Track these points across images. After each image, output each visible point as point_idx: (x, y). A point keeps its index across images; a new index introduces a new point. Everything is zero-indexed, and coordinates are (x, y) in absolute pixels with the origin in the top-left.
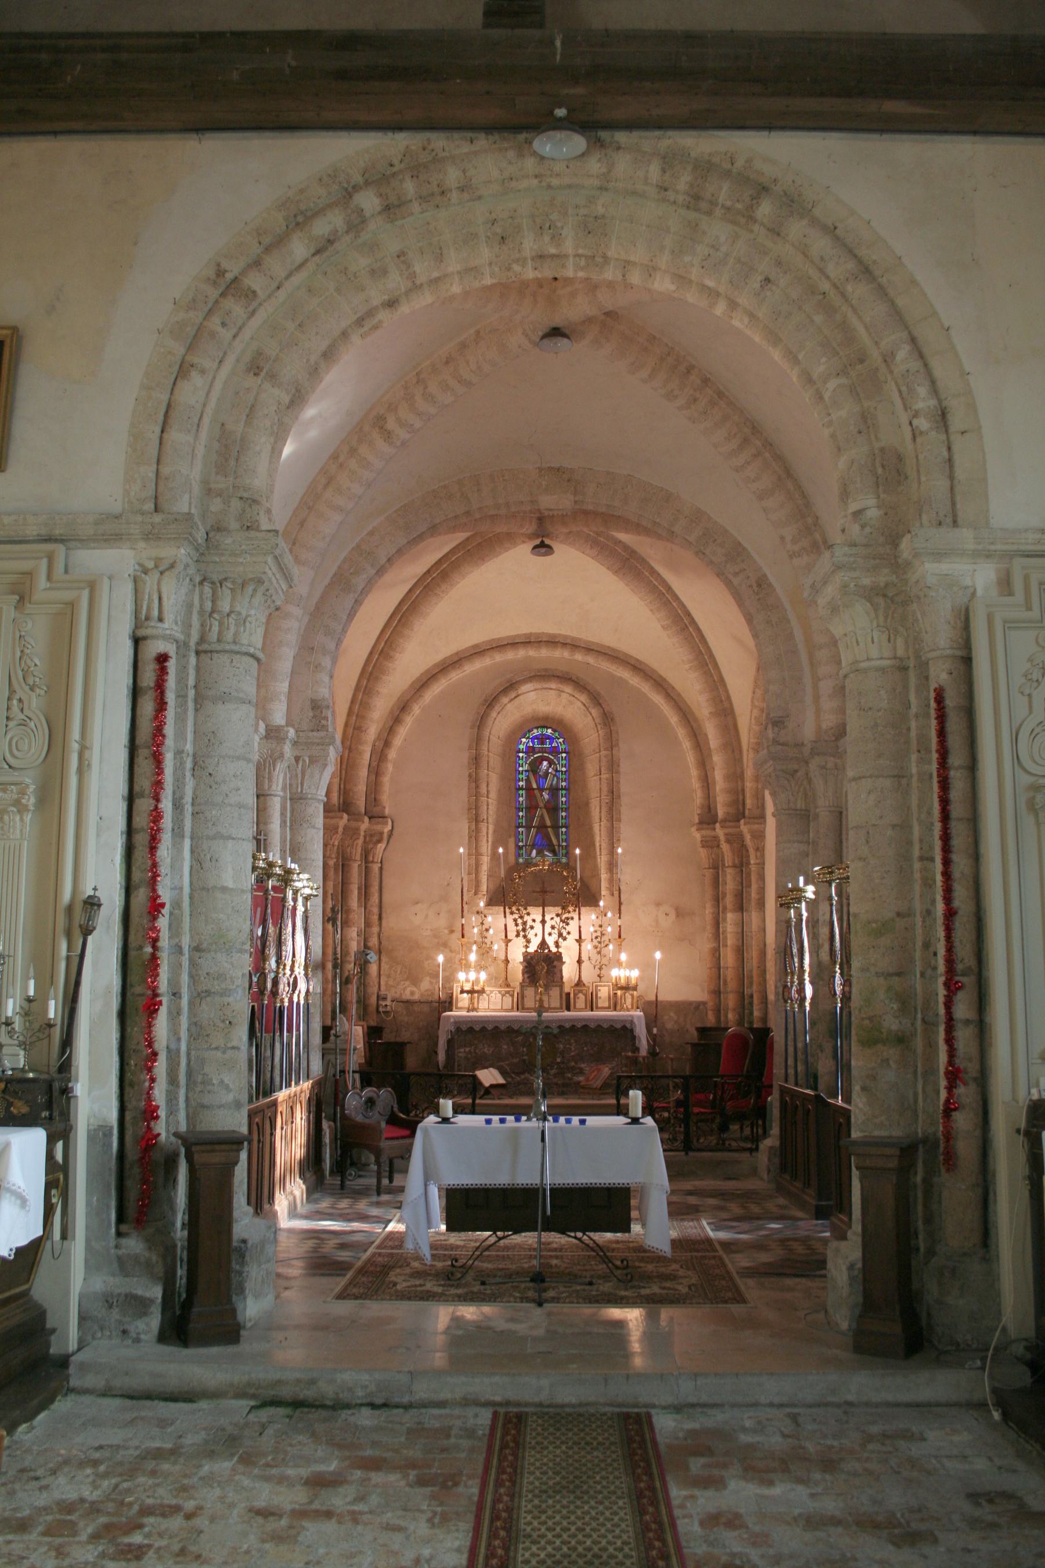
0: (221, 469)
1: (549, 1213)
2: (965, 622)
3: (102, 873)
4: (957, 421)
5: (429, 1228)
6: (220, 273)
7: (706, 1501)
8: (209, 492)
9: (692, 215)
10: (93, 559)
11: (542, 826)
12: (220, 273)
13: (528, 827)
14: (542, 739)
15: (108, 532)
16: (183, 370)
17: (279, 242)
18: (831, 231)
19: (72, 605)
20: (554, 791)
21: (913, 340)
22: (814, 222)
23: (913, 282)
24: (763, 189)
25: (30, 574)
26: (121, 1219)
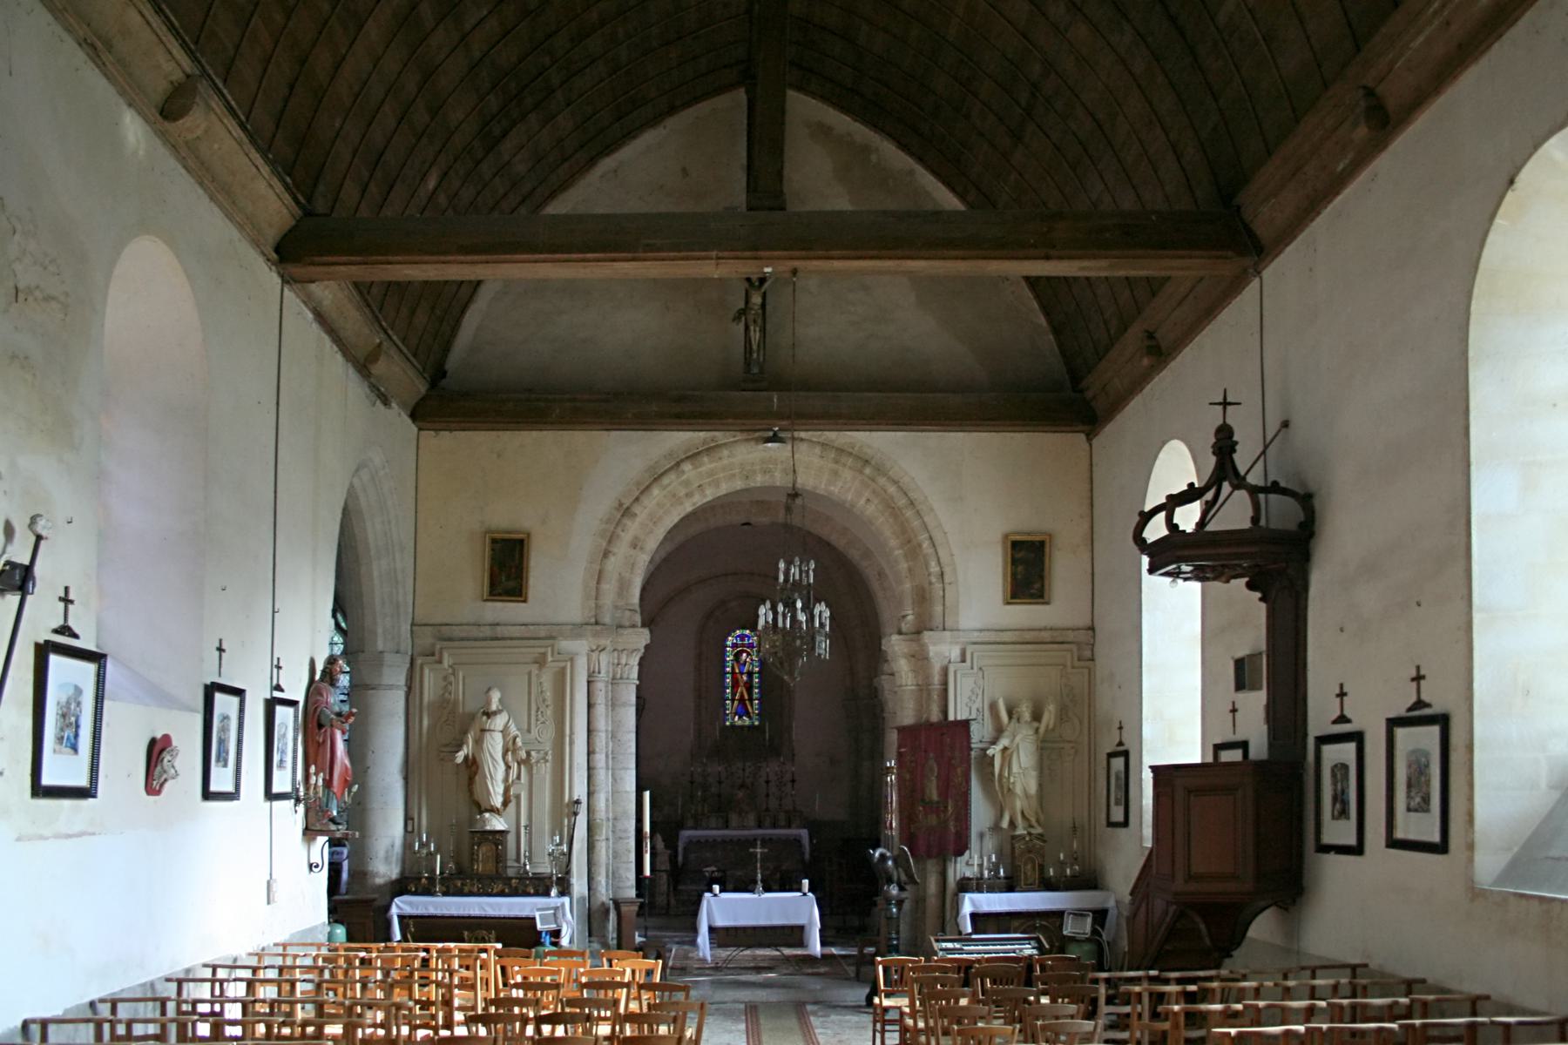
1: (647, 872)
2: (945, 672)
3: (580, 791)
5: (1164, 1034)
6: (621, 505)
8: (616, 607)
9: (835, 466)
10: (566, 645)
11: (742, 700)
12: (621, 505)
13: (733, 700)
14: (742, 637)
15: (577, 630)
16: (606, 554)
18: (895, 482)
19: (564, 669)
23: (932, 510)
24: (867, 462)
25: (544, 654)
26: (590, 935)
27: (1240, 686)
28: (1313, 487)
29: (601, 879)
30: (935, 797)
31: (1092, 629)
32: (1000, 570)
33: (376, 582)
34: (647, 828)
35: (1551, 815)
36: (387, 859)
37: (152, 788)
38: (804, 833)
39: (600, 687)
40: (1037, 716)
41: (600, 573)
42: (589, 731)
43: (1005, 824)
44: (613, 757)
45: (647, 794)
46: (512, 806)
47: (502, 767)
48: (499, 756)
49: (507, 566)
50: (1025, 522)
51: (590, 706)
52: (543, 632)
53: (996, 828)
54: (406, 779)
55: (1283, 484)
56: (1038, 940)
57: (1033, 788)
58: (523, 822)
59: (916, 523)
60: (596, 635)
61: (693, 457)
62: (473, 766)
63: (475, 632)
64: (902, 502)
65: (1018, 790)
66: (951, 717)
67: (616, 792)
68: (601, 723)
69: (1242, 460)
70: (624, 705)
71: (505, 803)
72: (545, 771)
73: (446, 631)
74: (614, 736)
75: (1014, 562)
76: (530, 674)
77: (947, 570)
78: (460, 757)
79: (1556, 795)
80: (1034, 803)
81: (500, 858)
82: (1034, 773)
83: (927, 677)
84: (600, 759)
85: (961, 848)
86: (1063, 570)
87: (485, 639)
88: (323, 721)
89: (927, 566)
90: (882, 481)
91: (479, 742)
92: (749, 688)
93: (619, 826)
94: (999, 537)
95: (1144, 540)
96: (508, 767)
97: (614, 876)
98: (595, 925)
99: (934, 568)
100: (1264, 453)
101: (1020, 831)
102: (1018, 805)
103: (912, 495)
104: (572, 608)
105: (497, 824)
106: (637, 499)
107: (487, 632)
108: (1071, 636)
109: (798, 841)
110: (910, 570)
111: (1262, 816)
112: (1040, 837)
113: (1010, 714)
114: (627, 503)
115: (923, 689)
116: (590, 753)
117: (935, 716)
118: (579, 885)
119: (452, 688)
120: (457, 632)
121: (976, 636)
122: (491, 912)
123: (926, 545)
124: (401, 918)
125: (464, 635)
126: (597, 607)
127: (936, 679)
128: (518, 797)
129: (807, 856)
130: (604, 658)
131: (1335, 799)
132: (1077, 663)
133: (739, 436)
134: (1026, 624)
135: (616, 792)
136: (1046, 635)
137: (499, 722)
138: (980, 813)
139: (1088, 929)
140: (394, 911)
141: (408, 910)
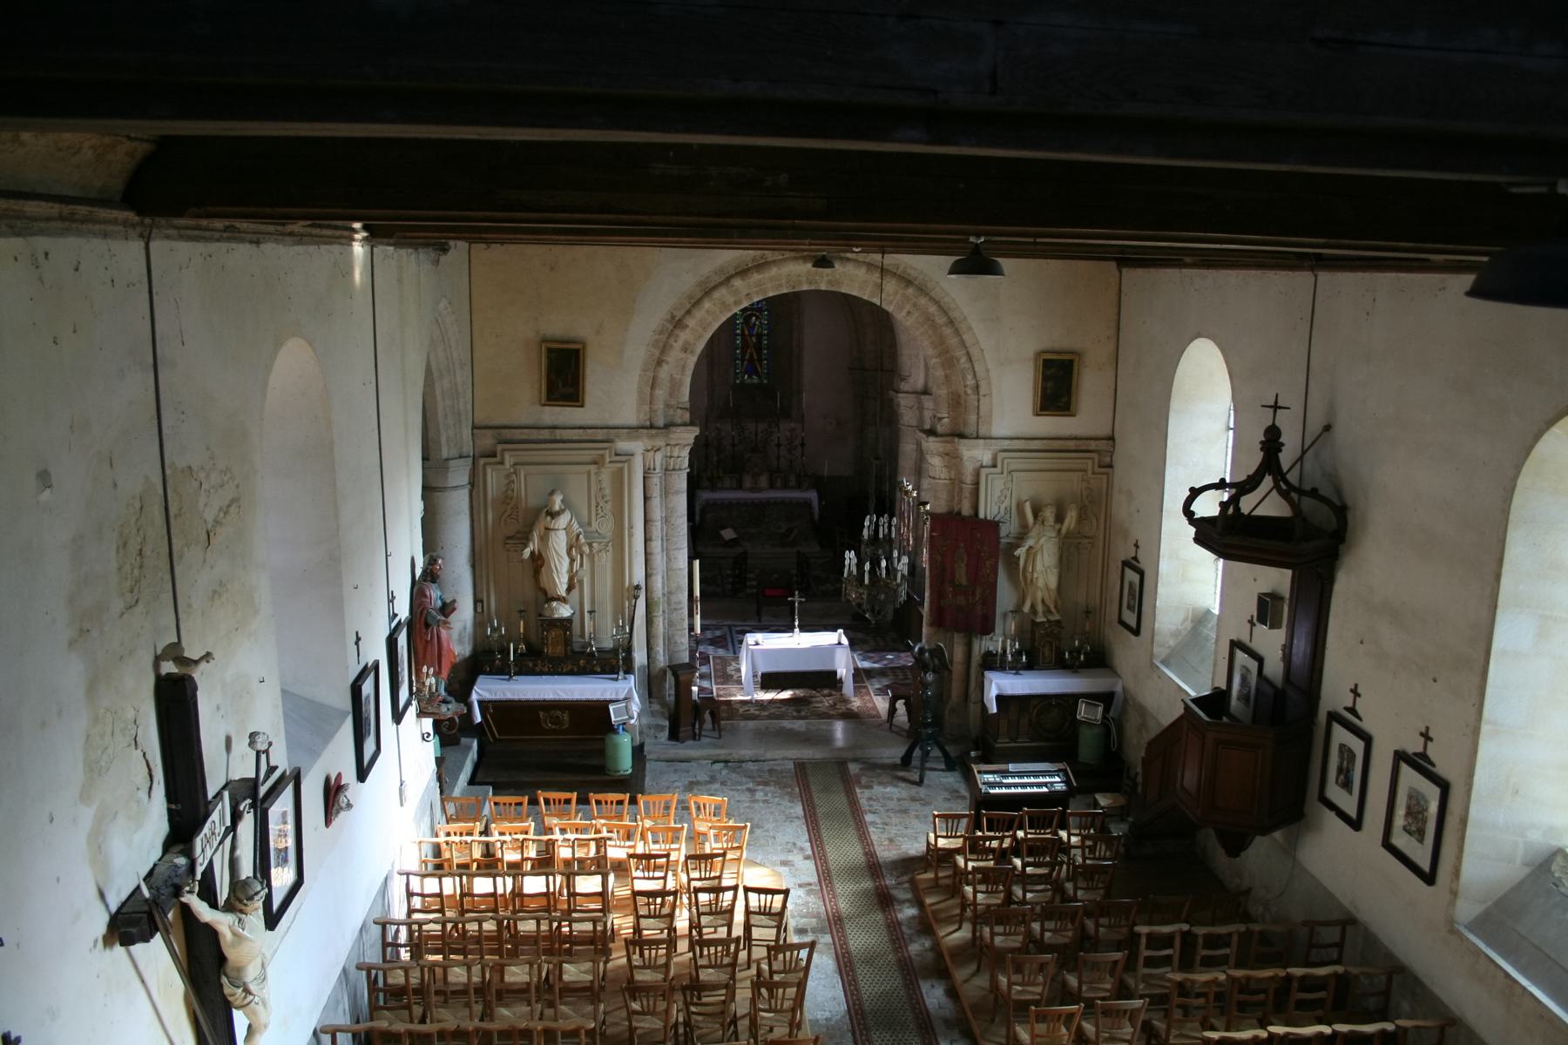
0: (671, 395)
2: (977, 474)
3: (639, 576)
4: (982, 391)
6: (673, 317)
7: (867, 793)
10: (623, 445)
11: (751, 360)
13: (743, 360)
15: (634, 430)
16: (659, 363)
17: (698, 302)
18: (937, 303)
19: (621, 469)
20: (759, 336)
21: (968, 354)
22: (931, 299)
23: (970, 328)
25: (602, 456)
26: (650, 696)
27: (1262, 618)
28: (1349, 504)
29: (660, 649)
30: (964, 581)
31: (1112, 438)
32: (1031, 385)
33: (439, 397)
34: (697, 593)
35: (1521, 884)
36: (460, 641)
37: (328, 822)
38: (812, 495)
39: (655, 480)
40: (1060, 518)
41: (654, 379)
42: (646, 522)
43: (1026, 609)
44: (667, 539)
45: (697, 563)
46: (575, 592)
47: (567, 560)
48: (563, 552)
49: (564, 373)
50: (1057, 339)
51: (646, 499)
52: (600, 434)
53: (1017, 610)
54: (473, 566)
55: (1321, 492)
56: (1064, 771)
57: (1053, 582)
58: (587, 608)
59: (954, 341)
60: (652, 437)
61: (743, 272)
62: (538, 561)
63: (534, 434)
64: (941, 320)
65: (1041, 583)
66: (982, 516)
67: (669, 570)
68: (657, 513)
69: (1286, 458)
70: (677, 492)
71: (569, 590)
72: (606, 560)
73: (507, 434)
74: (667, 520)
75: (1045, 378)
76: (589, 473)
77: (983, 385)
78: (527, 553)
79: (1527, 870)
80: (1054, 594)
81: (568, 642)
82: (1055, 571)
83: (960, 473)
84: (656, 545)
85: (987, 628)
86: (1090, 385)
87: (546, 442)
88: (430, 620)
89: (964, 378)
90: (923, 301)
91: (544, 539)
92: (759, 349)
93: (674, 599)
94: (1031, 355)
95: (1193, 513)
96: (572, 561)
97: (669, 641)
98: (654, 690)
99: (970, 381)
100: (1301, 458)
101: (1040, 619)
102: (1039, 595)
103: (954, 314)
104: (628, 411)
105: (564, 611)
106: (689, 312)
107: (546, 434)
108: (1093, 445)
109: (807, 504)
110: (946, 377)
111: (1275, 739)
112: (1058, 622)
113: (1036, 516)
114: (679, 315)
115: (956, 482)
116: (647, 540)
117: (966, 510)
118: (640, 657)
119: (515, 486)
120: (517, 434)
121: (1006, 444)
122: (564, 696)
123: (963, 360)
124: (481, 703)
125: (524, 437)
126: (651, 410)
127: (969, 478)
128: (581, 582)
129: (816, 516)
130: (659, 456)
131: (1340, 770)
132: (1097, 470)
133: (788, 254)
134: (1053, 432)
135: (669, 570)
136: (1071, 444)
137: (563, 520)
138: (1005, 596)
139: (1099, 716)
140: (474, 697)
141: (487, 696)
